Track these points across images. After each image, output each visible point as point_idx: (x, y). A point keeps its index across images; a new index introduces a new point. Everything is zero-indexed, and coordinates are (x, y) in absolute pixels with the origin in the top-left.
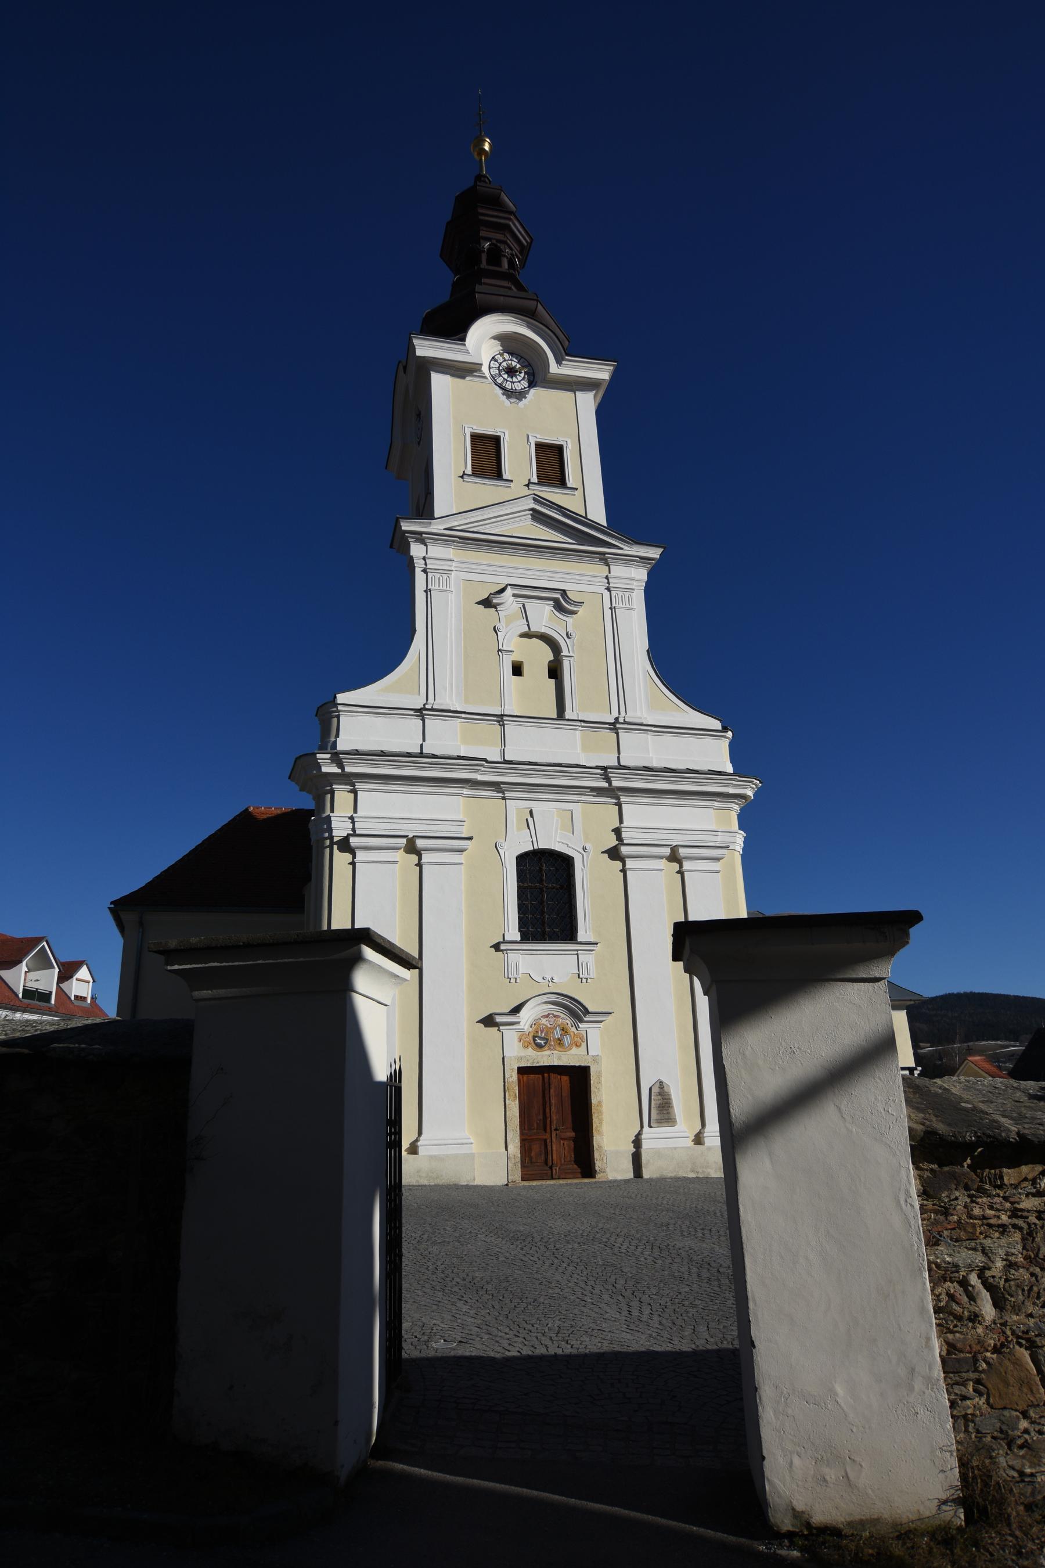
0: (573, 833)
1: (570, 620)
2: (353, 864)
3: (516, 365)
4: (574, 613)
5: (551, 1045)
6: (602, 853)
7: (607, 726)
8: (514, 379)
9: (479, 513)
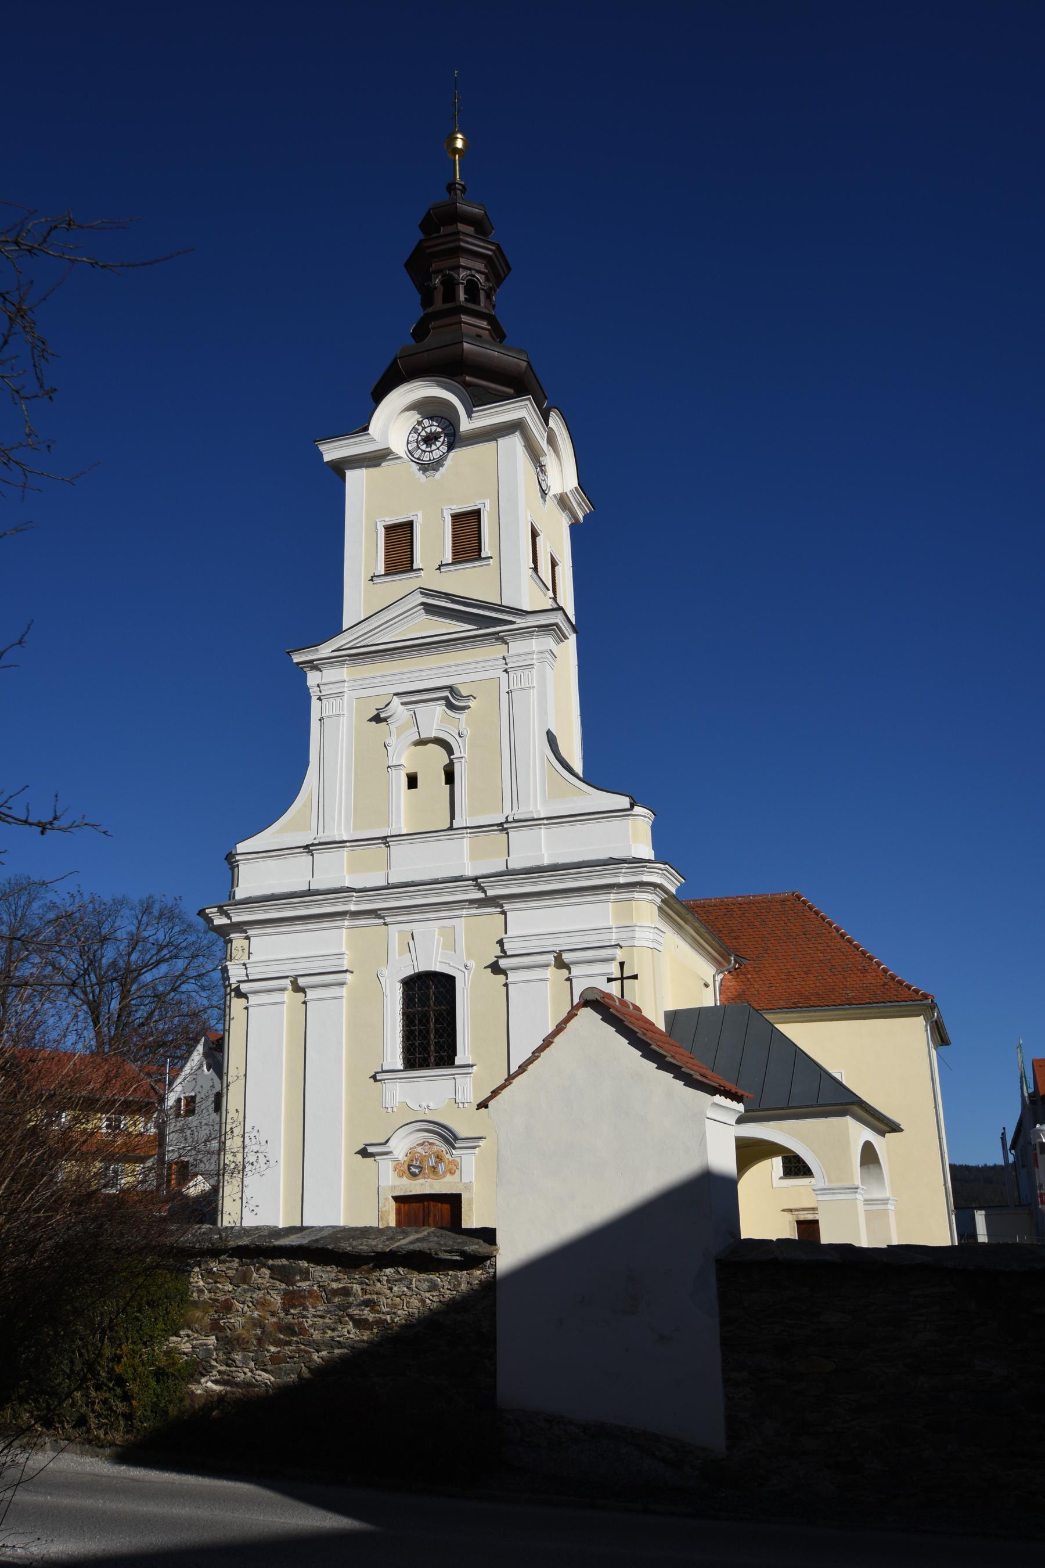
0: (455, 951)
1: (463, 716)
2: (506, 985)
3: (431, 430)
4: (468, 707)
5: (426, 1174)
6: (485, 968)
7: (496, 828)
8: (434, 447)
9: (365, 625)
